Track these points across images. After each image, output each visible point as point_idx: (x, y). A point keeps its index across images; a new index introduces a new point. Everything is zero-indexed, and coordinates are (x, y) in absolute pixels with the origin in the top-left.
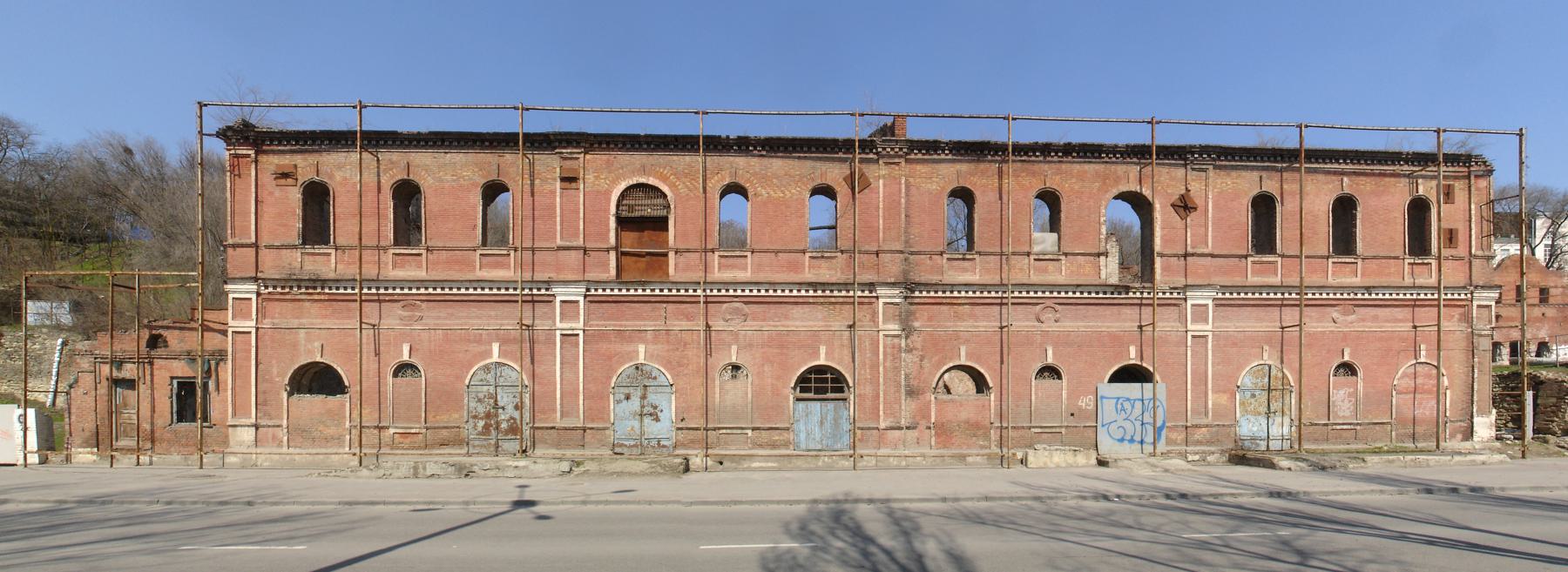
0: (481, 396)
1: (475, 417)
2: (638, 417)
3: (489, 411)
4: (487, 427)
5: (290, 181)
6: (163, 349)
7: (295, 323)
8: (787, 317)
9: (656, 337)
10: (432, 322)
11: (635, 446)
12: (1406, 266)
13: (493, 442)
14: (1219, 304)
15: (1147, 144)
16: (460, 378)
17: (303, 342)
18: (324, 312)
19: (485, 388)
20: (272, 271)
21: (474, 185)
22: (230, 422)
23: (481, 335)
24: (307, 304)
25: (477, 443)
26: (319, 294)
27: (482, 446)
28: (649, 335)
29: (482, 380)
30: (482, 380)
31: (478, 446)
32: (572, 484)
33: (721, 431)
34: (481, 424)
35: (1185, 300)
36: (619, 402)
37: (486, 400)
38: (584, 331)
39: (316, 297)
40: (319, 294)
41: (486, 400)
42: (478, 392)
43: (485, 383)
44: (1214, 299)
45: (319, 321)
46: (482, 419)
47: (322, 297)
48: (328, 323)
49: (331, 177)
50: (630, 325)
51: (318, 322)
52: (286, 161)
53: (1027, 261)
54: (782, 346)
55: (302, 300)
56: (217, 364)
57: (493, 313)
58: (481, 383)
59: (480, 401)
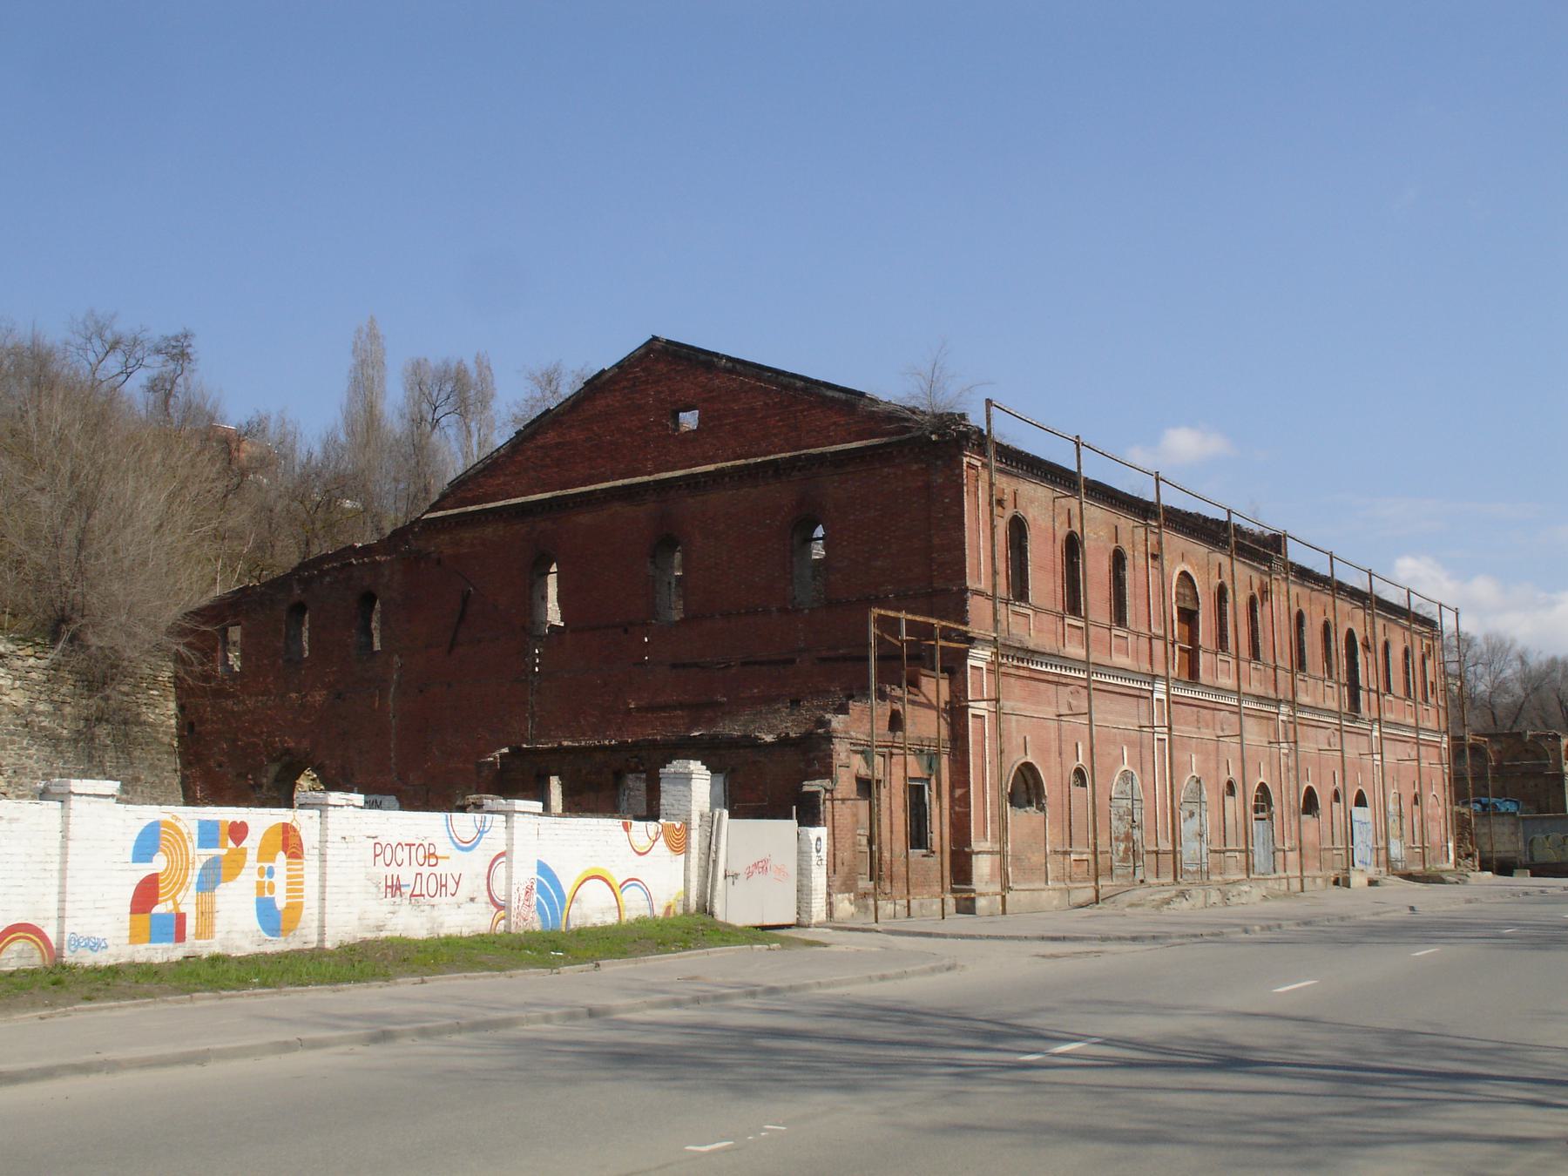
34: (1122, 846)
45: (1021, 705)
46: (1122, 841)
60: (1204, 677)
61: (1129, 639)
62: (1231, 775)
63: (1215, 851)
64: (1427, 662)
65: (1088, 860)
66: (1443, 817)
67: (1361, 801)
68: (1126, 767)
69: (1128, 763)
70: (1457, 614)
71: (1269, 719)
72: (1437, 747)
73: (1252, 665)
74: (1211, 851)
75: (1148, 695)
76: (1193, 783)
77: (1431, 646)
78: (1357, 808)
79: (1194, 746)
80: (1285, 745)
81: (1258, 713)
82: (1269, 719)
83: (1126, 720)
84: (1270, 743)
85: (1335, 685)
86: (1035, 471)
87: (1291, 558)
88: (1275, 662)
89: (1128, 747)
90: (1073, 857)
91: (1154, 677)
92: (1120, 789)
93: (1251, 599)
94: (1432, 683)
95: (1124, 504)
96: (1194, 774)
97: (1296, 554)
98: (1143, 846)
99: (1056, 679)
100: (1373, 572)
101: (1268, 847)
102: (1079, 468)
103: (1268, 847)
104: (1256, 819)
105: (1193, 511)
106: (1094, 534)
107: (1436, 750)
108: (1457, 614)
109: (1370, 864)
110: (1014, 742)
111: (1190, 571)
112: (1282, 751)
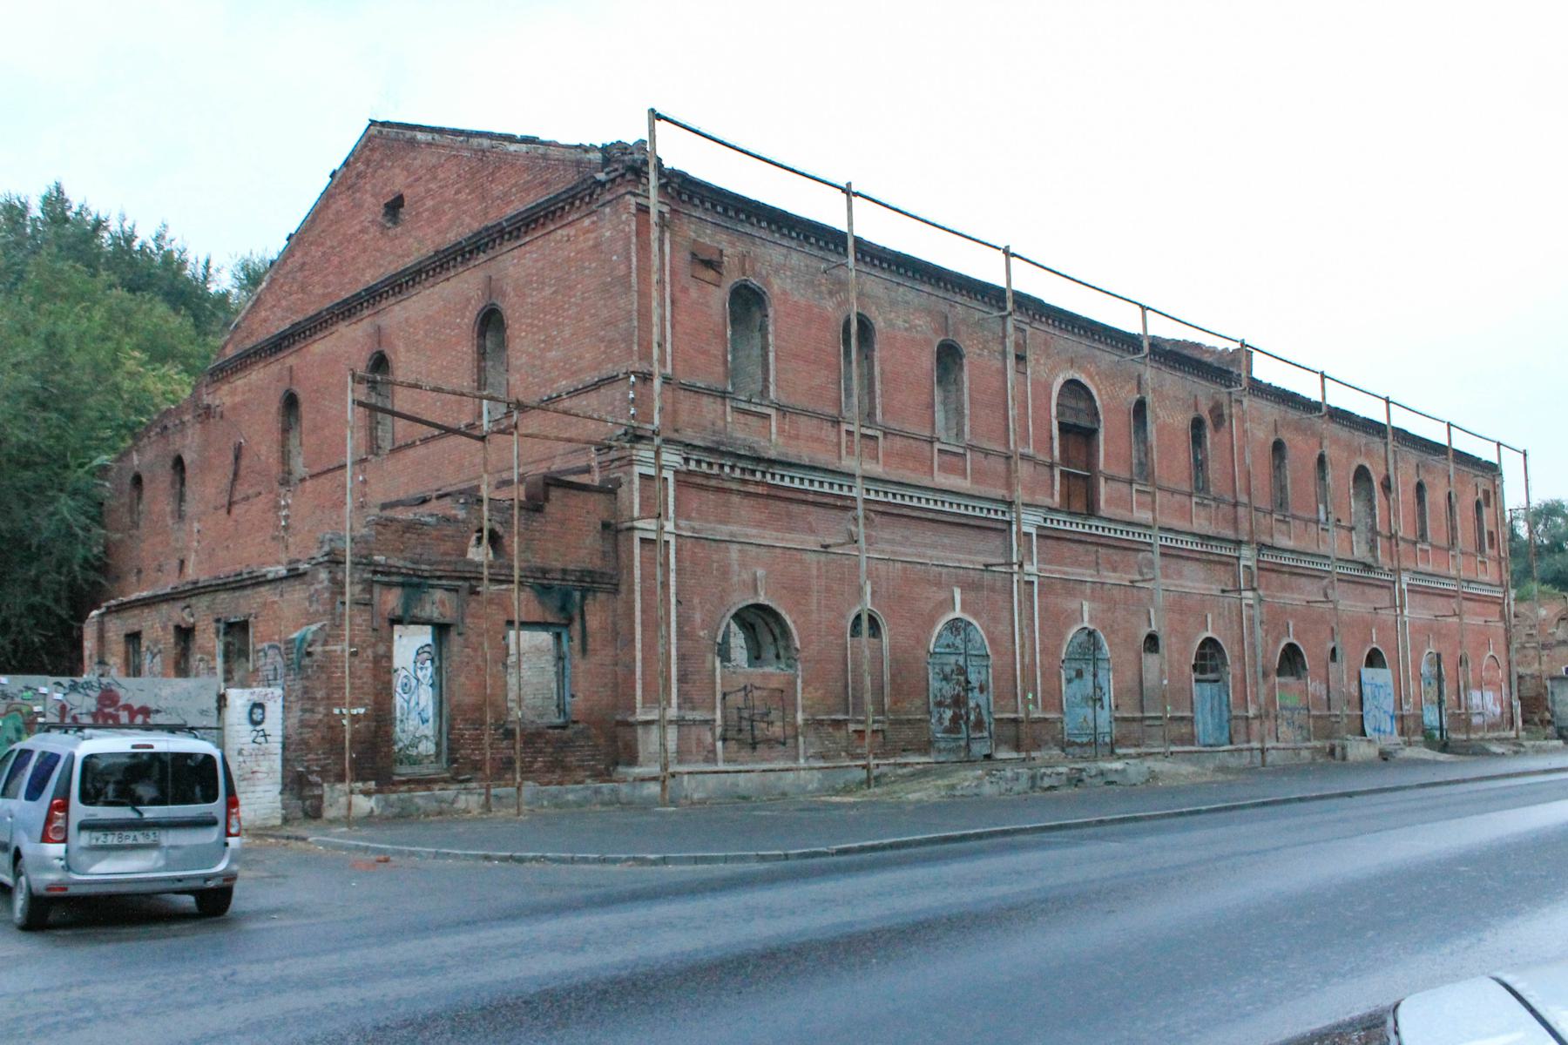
0: (948, 669)
1: (939, 704)
2: (1091, 703)
3: (958, 695)
4: (955, 719)
5: (710, 275)
6: (571, 567)
7: (723, 531)
8: (1180, 575)
9: (1093, 591)
10: (888, 548)
11: (1089, 744)
12: (844, 434)
13: (963, 743)
14: (684, 480)
15: (630, 140)
16: (921, 641)
17: (736, 567)
18: (757, 516)
19: (952, 659)
20: (689, 432)
21: (928, 342)
22: (641, 716)
23: (940, 574)
24: (735, 499)
25: (942, 745)
26: (757, 483)
27: (950, 750)
28: (1088, 589)
29: (948, 646)
30: (948, 646)
31: (945, 749)
32: (605, 861)
33: (1148, 722)
34: (948, 714)
35: (1238, 558)
36: (1069, 681)
37: (954, 677)
38: (678, 536)
39: (751, 488)
40: (757, 483)
41: (954, 677)
42: (942, 664)
43: (952, 650)
44: (1039, 527)
45: (754, 531)
46: (948, 706)
47: (760, 490)
48: (769, 537)
49: (768, 283)
50: (1075, 573)
51: (753, 533)
52: (713, 238)
53: (719, 407)
54: (1182, 612)
55: (730, 491)
56: (583, 598)
57: (946, 541)
58: (948, 650)
59: (946, 678)
60: (1104, 508)
61: (968, 456)
62: (1154, 628)
63: (1125, 719)
64: (1485, 510)
65: (883, 731)
66: (1505, 679)
67: (1374, 659)
68: (958, 613)
69: (963, 608)
70: (1525, 455)
71: (1227, 564)
72: (1389, 588)
73: (1195, 499)
74: (1116, 719)
75: (1005, 526)
76: (1083, 637)
77: (1491, 493)
78: (1370, 670)
79: (1088, 591)
80: (1249, 594)
81: (1204, 557)
82: (1227, 564)
83: (961, 556)
84: (1223, 591)
85: (1212, 503)
86: (785, 231)
87: (1256, 374)
88: (1235, 496)
89: (963, 589)
90: (852, 727)
91: (1239, 543)
92: (943, 641)
93: (1193, 427)
94: (1491, 534)
95: (1047, 318)
96: (1086, 624)
97: (1263, 370)
98: (990, 713)
99: (1216, 558)
100: (1012, 250)
101: (1221, 715)
102: (850, 224)
103: (1221, 715)
104: (1197, 681)
105: (1265, 381)
106: (905, 321)
107: (1498, 608)
108: (1525, 455)
109: (1391, 733)
110: (735, 579)
111: (1084, 379)
112: (1244, 602)
